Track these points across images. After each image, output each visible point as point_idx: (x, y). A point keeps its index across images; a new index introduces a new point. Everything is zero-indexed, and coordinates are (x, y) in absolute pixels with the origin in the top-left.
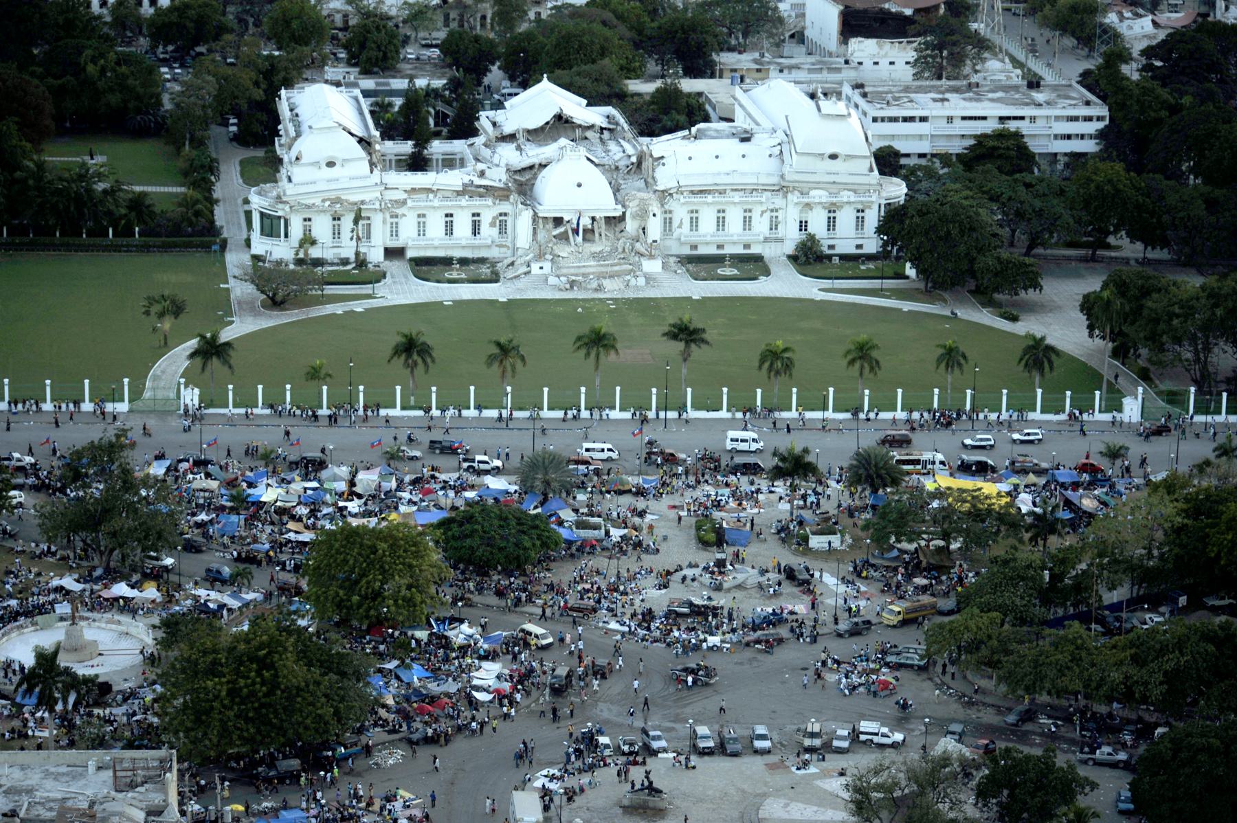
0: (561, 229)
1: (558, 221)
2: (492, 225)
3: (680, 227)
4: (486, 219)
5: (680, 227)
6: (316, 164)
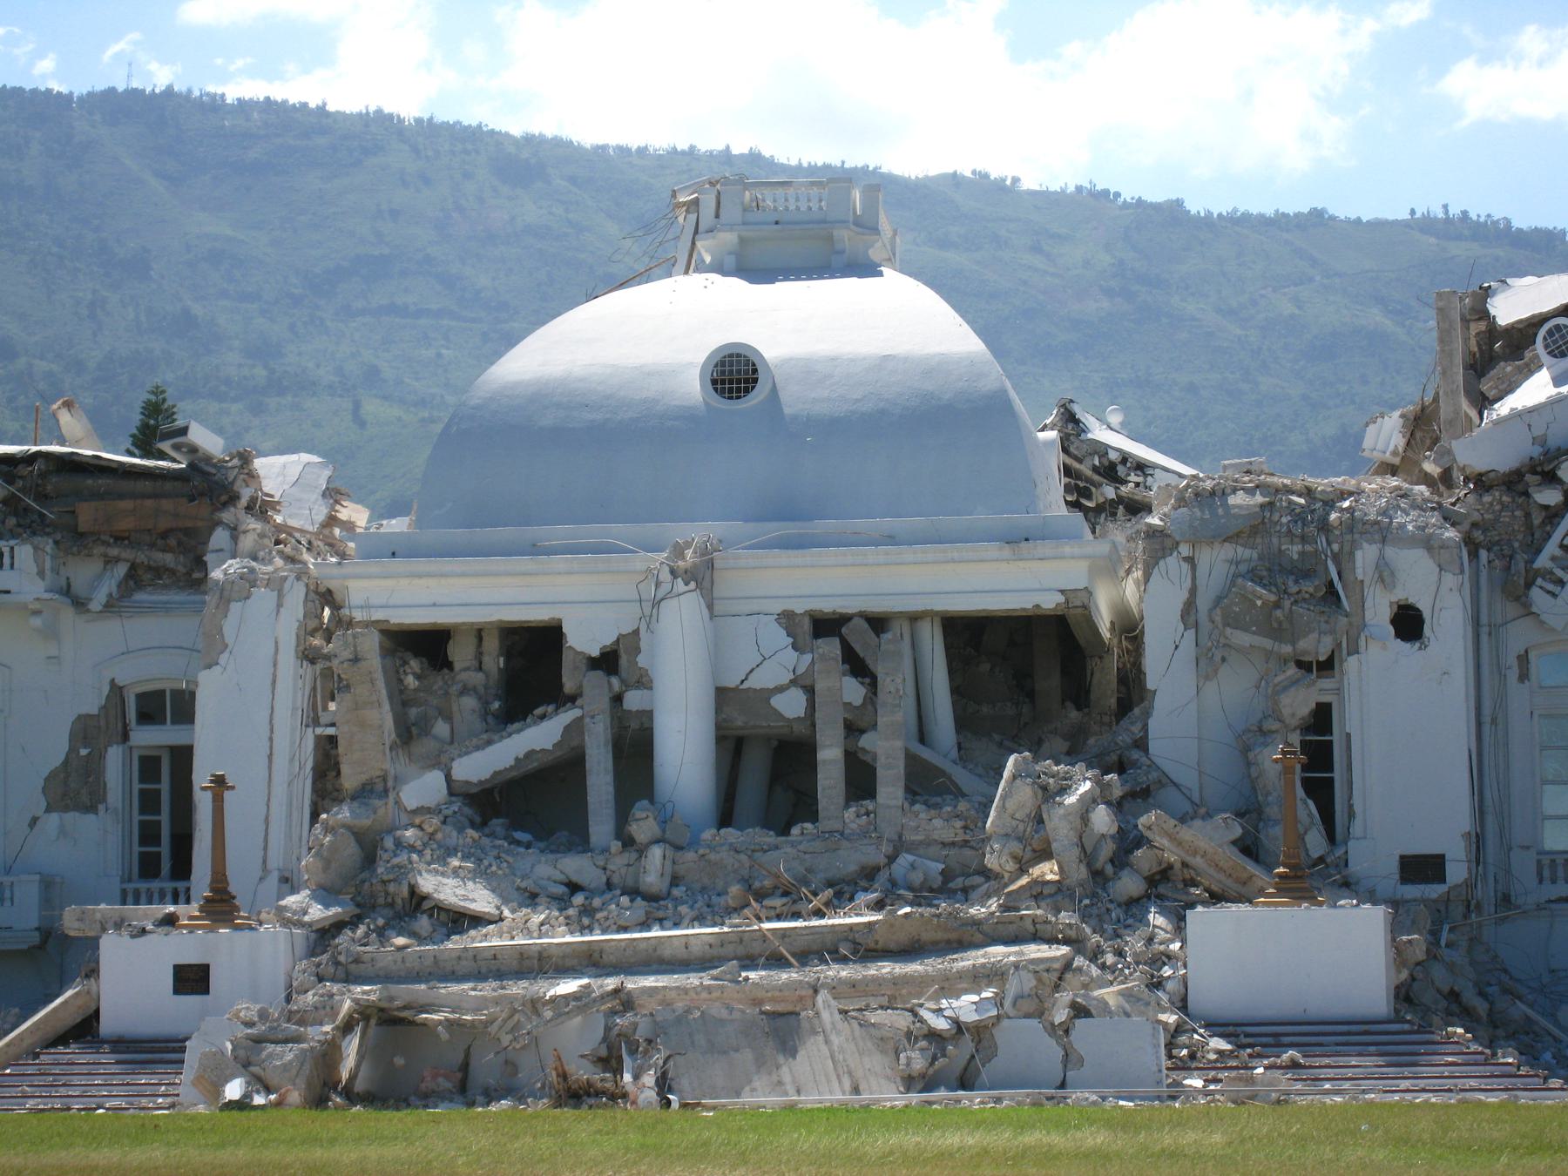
0: (541, 735)
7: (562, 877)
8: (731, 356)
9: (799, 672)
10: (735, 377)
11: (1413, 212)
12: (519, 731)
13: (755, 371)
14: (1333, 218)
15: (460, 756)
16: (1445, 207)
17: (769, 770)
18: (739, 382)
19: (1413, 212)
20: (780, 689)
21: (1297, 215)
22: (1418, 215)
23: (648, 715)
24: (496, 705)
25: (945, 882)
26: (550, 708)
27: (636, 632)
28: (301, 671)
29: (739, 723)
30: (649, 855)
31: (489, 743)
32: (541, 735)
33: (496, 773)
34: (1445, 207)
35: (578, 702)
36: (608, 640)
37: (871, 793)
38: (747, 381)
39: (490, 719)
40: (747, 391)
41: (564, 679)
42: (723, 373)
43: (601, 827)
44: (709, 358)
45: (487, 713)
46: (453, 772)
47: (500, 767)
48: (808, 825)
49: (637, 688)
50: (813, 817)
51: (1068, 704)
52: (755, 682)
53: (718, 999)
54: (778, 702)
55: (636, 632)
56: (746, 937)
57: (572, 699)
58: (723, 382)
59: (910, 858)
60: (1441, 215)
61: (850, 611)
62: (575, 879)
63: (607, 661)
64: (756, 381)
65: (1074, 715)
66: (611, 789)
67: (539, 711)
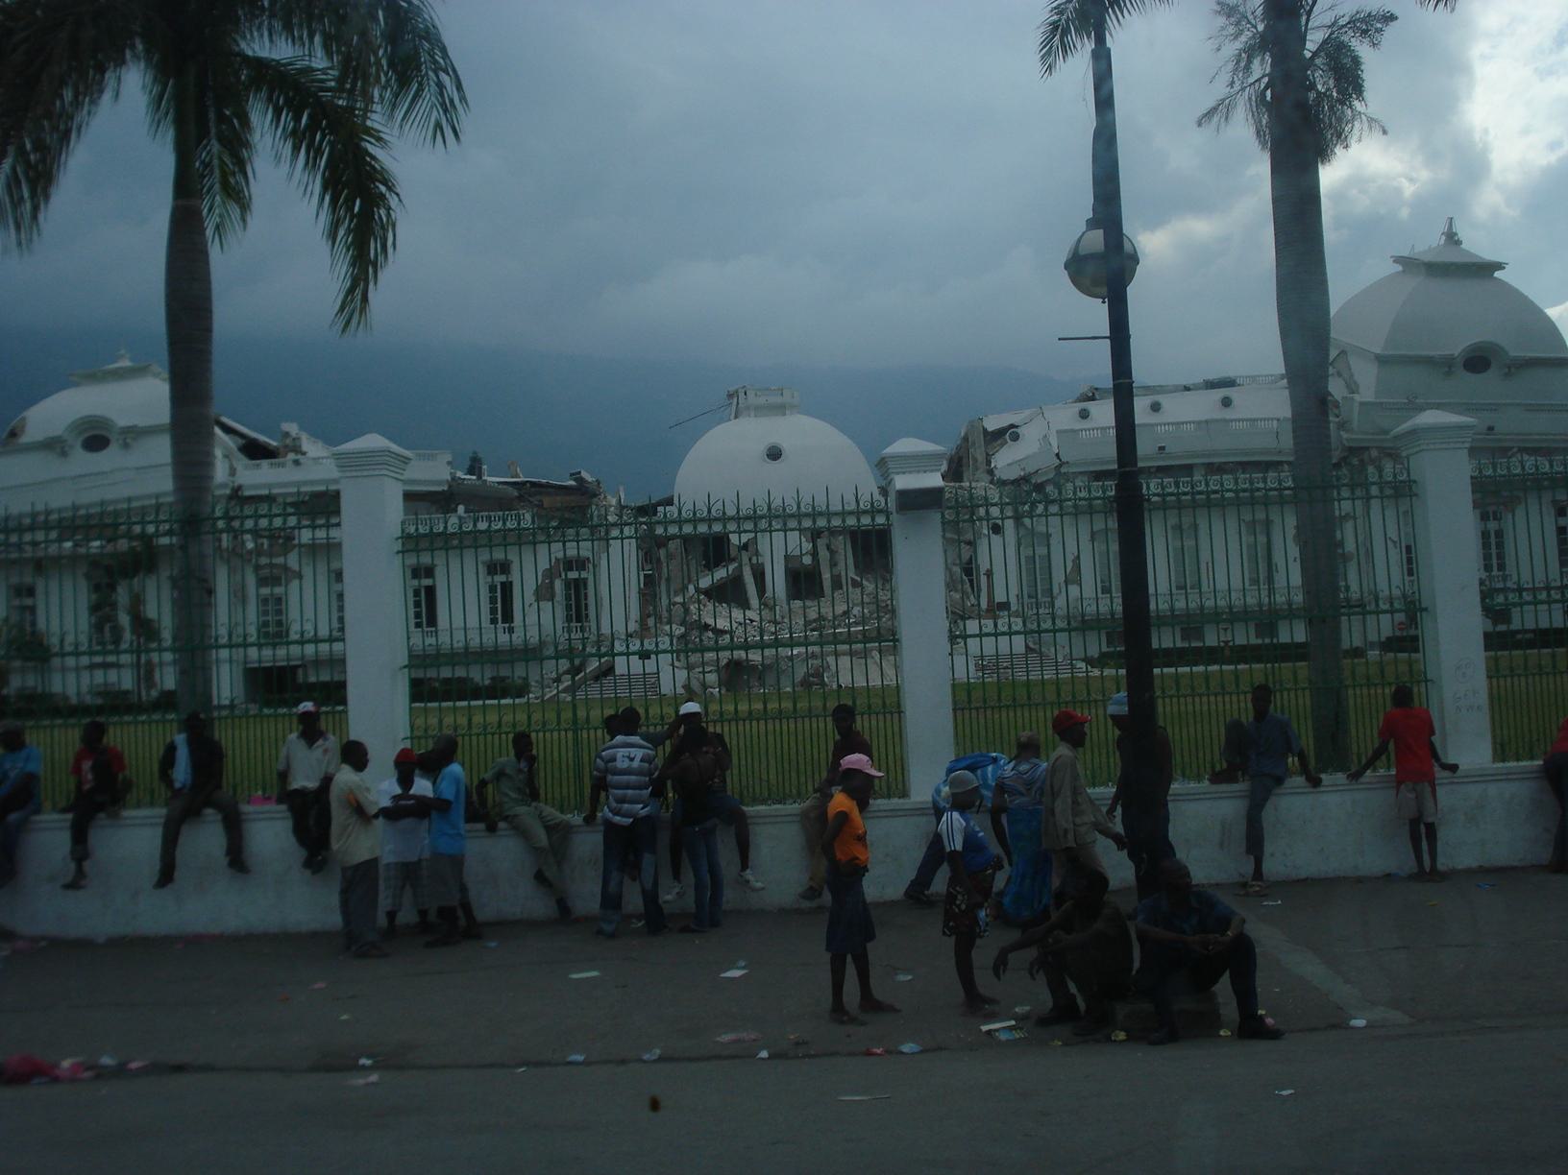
1: (715, 550)
2: (544, 593)
3: (1074, 577)
4: (529, 570)
5: (1074, 577)
6: (54, 446)
63: (745, 547)
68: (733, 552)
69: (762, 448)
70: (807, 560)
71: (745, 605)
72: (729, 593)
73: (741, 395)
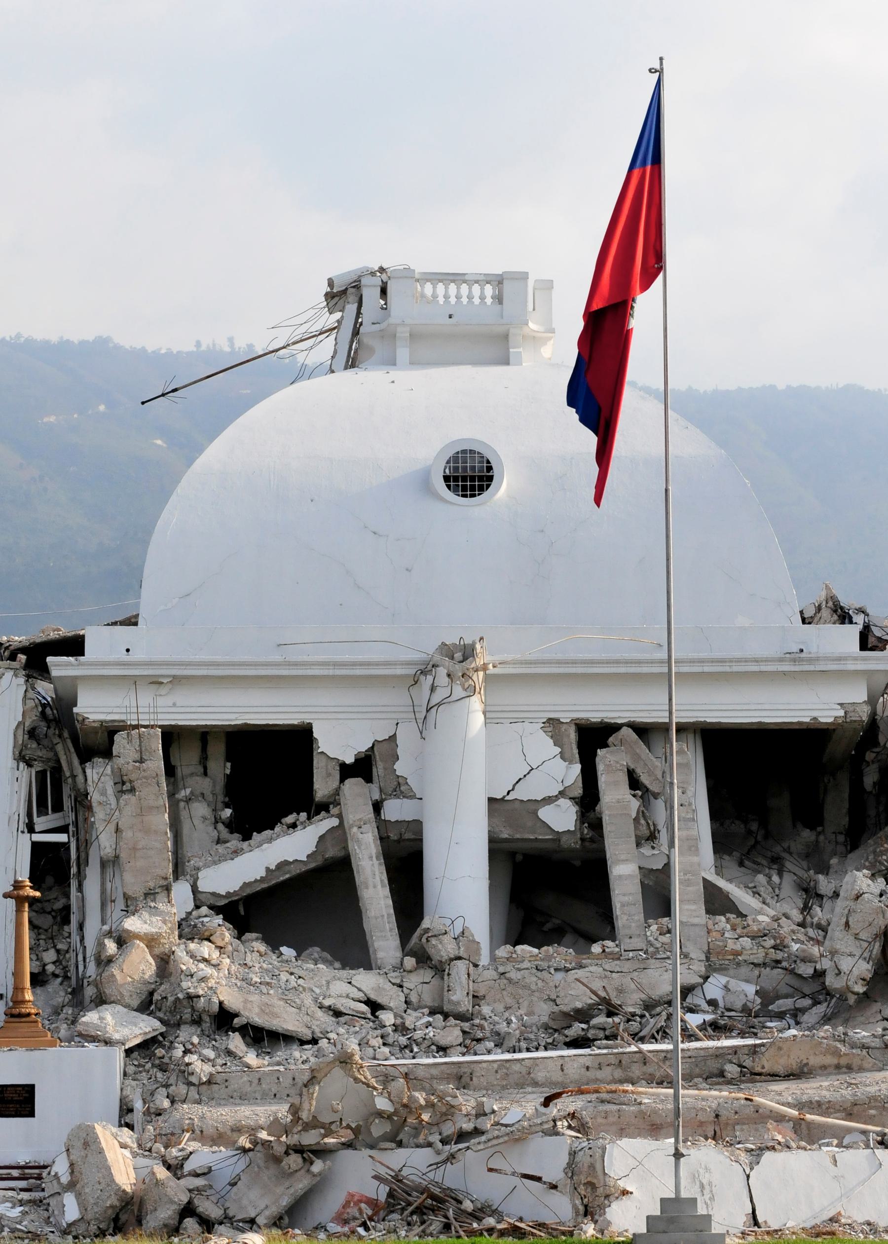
0: (292, 846)
1: (265, 772)
7: (360, 995)
8: (464, 452)
9: (567, 784)
10: (469, 473)
11: (198, 344)
12: (270, 840)
13: (490, 468)
14: (117, 347)
15: (207, 866)
16: (231, 340)
17: (552, 888)
18: (472, 479)
19: (198, 344)
20: (548, 800)
21: (82, 343)
22: (204, 348)
23: (416, 826)
24: (228, 812)
25: (765, 1004)
26: (303, 815)
27: (393, 738)
28: (17, 774)
29: (505, 836)
30: (453, 973)
31: (237, 852)
32: (292, 846)
33: (245, 885)
34: (231, 340)
35: (334, 810)
36: (363, 746)
37: (667, 911)
38: (481, 478)
39: (220, 826)
40: (482, 489)
41: (316, 786)
42: (456, 469)
43: (384, 937)
44: (442, 450)
45: (216, 822)
46: (199, 883)
47: (250, 878)
48: (609, 943)
49: (397, 797)
50: (612, 936)
51: (799, 826)
52: (522, 793)
53: (614, 1123)
54: (546, 814)
55: (393, 738)
56: (625, 1059)
57: (324, 807)
58: (456, 479)
59: (723, 980)
60: (227, 349)
61: (620, 721)
62: (373, 996)
63: (361, 768)
64: (490, 479)
65: (807, 835)
66: (390, 902)
67: (290, 819)
68: (323, 785)
69: (430, 452)
70: (562, 818)
71: (353, 952)
72: (298, 912)
73: (371, 295)
